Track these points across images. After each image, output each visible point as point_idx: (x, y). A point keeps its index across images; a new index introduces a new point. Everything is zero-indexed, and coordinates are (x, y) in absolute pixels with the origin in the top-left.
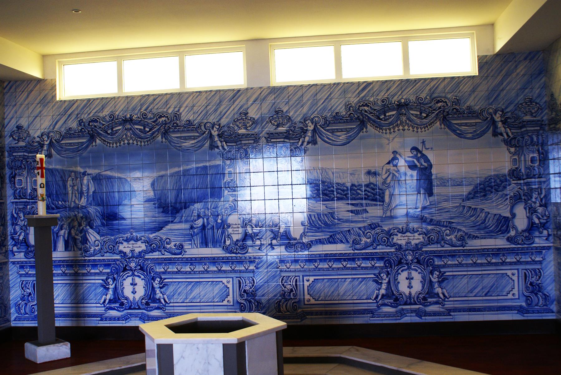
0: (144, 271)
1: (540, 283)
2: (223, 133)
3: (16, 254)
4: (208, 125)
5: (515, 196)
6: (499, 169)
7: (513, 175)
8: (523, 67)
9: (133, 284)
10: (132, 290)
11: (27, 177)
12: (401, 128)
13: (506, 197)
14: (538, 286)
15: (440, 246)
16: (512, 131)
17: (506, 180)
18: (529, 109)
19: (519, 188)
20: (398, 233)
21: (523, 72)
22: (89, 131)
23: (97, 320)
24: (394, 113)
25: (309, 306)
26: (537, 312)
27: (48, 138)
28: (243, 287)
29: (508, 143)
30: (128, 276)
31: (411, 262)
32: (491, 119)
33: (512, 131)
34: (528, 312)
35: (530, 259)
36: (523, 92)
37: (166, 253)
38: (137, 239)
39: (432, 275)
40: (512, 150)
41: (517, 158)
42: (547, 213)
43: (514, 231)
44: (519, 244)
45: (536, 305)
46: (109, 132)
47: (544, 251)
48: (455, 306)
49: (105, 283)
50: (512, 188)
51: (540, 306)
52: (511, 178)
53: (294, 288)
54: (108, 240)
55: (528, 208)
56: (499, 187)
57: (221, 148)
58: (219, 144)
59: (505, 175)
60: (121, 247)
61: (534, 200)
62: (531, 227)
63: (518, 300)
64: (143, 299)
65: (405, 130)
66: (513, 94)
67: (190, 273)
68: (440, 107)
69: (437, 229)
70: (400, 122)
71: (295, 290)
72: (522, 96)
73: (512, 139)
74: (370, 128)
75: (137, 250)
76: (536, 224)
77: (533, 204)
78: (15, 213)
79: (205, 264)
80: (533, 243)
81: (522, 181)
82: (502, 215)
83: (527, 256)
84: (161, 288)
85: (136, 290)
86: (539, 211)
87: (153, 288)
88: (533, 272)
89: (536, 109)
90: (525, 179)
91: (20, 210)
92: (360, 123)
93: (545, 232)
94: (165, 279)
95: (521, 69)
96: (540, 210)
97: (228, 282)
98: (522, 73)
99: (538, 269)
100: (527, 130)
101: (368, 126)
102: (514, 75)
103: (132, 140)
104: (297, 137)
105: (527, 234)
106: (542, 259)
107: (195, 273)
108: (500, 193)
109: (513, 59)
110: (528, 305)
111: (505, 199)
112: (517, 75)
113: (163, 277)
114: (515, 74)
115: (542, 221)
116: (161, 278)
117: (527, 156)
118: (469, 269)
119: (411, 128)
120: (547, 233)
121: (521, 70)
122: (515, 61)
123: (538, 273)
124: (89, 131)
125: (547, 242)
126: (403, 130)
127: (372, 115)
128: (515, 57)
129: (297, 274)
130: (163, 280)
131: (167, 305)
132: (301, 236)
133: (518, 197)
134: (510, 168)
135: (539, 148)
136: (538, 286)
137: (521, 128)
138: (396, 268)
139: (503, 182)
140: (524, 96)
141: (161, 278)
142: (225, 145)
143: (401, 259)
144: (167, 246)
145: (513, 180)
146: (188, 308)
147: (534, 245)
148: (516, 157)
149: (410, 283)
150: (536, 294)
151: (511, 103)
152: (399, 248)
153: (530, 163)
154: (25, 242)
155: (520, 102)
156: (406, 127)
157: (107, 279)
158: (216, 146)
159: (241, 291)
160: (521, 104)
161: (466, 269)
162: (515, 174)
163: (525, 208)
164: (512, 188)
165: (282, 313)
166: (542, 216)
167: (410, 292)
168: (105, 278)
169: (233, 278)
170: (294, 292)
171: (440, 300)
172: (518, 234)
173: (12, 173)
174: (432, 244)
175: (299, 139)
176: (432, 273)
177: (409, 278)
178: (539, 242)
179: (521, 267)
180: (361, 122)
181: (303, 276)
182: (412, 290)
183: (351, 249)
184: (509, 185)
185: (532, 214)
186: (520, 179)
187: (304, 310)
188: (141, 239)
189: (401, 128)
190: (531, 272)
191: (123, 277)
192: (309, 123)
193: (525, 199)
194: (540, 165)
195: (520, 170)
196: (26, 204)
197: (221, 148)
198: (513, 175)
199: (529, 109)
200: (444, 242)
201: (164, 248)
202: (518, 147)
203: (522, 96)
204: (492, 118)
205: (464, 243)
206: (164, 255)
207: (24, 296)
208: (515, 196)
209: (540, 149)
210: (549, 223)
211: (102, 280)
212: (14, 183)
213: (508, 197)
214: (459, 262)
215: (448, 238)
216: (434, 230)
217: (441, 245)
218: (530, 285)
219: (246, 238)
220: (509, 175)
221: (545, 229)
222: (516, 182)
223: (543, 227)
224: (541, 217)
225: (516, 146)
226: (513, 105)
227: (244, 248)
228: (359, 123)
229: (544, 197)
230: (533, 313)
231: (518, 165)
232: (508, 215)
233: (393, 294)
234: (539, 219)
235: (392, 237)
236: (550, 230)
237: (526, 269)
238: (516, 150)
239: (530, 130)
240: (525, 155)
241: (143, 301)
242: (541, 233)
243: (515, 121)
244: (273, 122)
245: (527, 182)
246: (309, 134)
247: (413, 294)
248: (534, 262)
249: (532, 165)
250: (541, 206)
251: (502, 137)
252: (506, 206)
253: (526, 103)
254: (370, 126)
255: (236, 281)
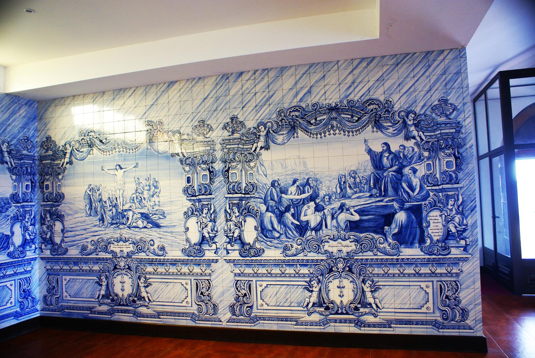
0: (132, 271)
1: (30, 289)
2: (419, 122)
3: (230, 252)
4: (403, 113)
5: (14, 216)
6: (4, 193)
7: (13, 199)
8: (24, 110)
9: (340, 287)
10: (339, 293)
11: (241, 171)
12: (332, 132)
13: (8, 218)
14: (28, 291)
15: (373, 255)
16: (15, 161)
17: (9, 203)
18: (26, 145)
19: (17, 210)
20: (329, 240)
21: (25, 113)
22: (289, 122)
23: (292, 324)
24: (324, 117)
25: (262, 311)
26: (27, 313)
27: (265, 129)
28: (444, 293)
29: (11, 170)
30: (118, 275)
31: (342, 270)
32: (403, 122)
33: (14, 161)
34: (444, 327)
35: (23, 270)
36: (23, 130)
37: (379, 254)
38: (345, 238)
39: (365, 284)
40: (14, 177)
41: (432, 163)
42: (35, 231)
43: (13, 246)
44: (16, 258)
45: (27, 308)
46: (313, 121)
47: (32, 262)
48: (428, 318)
49: (309, 285)
50: (13, 210)
51: (456, 321)
52: (12, 201)
53: (248, 293)
54: (312, 238)
55: (22, 227)
56: (3, 208)
57: (9, 163)
58: (415, 133)
59: (8, 199)
60: (327, 247)
61: (27, 220)
62: (25, 243)
63: (433, 315)
64: (351, 303)
65: (336, 134)
66: (16, 130)
67: (240, 276)
68: (372, 109)
69: (370, 236)
70: (331, 126)
71: (249, 295)
72: (22, 134)
73: (14, 168)
74: (300, 133)
75: (126, 250)
76: (27, 240)
77: (26, 224)
78: (44, 214)
79: (282, 267)
80: (25, 256)
81: (19, 205)
82: (4, 233)
83: (21, 268)
84: (371, 291)
85: (344, 293)
86: (30, 229)
87: (363, 292)
88: (25, 281)
89: (451, 110)
90: (197, 196)
91: (234, 204)
92: (291, 129)
93: (33, 246)
94: (378, 282)
95: (23, 111)
96: (31, 228)
97: (427, 287)
98: (23, 115)
99: (29, 277)
100: (24, 162)
101: (299, 131)
102: (18, 115)
103: (339, 130)
104: (250, 143)
105: (22, 249)
106: (459, 272)
107: (420, 275)
108: (4, 214)
109: (18, 101)
110: (22, 309)
111: (7, 219)
112: (20, 115)
113: (374, 279)
114: (18, 114)
115: (211, 235)
116: (373, 281)
117: (23, 184)
118: (411, 280)
119: (342, 132)
120: (465, 243)
121: (23, 113)
122: (19, 104)
123: (28, 280)
124: (289, 122)
125: (35, 254)
126: (333, 134)
127: (304, 120)
128: (19, 100)
129: (250, 279)
130: (375, 283)
131: (379, 310)
132: (255, 242)
133: (17, 218)
134: (11, 193)
135: (455, 152)
136: (28, 291)
137: (21, 159)
138: (327, 276)
139: (6, 205)
140: (24, 134)
141: (373, 281)
142: (422, 135)
143: (332, 267)
144: (380, 245)
145: (13, 203)
146: (279, 312)
147: (26, 258)
148: (16, 184)
149: (123, 286)
150: (27, 299)
151: (14, 138)
152: (330, 255)
153: (25, 190)
154: (240, 239)
155: (21, 139)
156: (337, 131)
157: (310, 281)
158: (412, 136)
159: (443, 297)
160: (21, 140)
161: (408, 280)
162: (14, 198)
163: (21, 227)
164: (13, 210)
165: (237, 316)
166: (32, 233)
167: (341, 301)
168: (308, 279)
169: (433, 281)
170: (248, 296)
171: (373, 310)
172: (16, 249)
173: (226, 167)
174: (140, 252)
175: (253, 145)
176: (364, 281)
177: (340, 287)
178: (455, 253)
179: (435, 279)
180: (292, 127)
181: (256, 281)
182: (343, 299)
183: (80, 254)
184: (11, 207)
185: (25, 231)
186: (18, 203)
187: (257, 314)
188: (129, 240)
189: (332, 132)
190: (24, 281)
191: (113, 276)
192: (262, 128)
193: (21, 220)
194: (31, 192)
195: (19, 195)
196: (241, 199)
197: (9, 163)
198: (13, 199)
199: (26, 145)
200: (377, 251)
201: (376, 247)
202: (18, 175)
203: (22, 134)
204: (404, 122)
205: (165, 253)
206: (148, 255)
207: (239, 297)
208: (14, 216)
209: (457, 153)
210: (36, 238)
211: (306, 282)
212: (228, 178)
213: (10, 217)
214: (432, 272)
215: (382, 246)
216: (367, 237)
217: (146, 254)
218: (445, 298)
219: (25, 244)
220: (11, 198)
221: (34, 244)
222: (15, 205)
223: (32, 242)
224: (31, 234)
225: (16, 175)
226: (15, 140)
227: (201, 252)
228: (290, 128)
229: (461, 204)
230: (25, 315)
231: (432, 170)
232: (8, 233)
233: (324, 303)
234: (30, 235)
235: (323, 244)
236: (36, 244)
237: (20, 279)
238: (16, 177)
239: (26, 163)
240: (22, 183)
241: (352, 305)
242: (31, 247)
243: (17, 153)
244: (228, 128)
245: (23, 205)
246: (262, 139)
247: (345, 303)
248: (26, 272)
249: (447, 170)
250: (31, 225)
251: (179, 157)
252: (8, 226)
253: (25, 140)
254: (301, 131)
255: (437, 285)
